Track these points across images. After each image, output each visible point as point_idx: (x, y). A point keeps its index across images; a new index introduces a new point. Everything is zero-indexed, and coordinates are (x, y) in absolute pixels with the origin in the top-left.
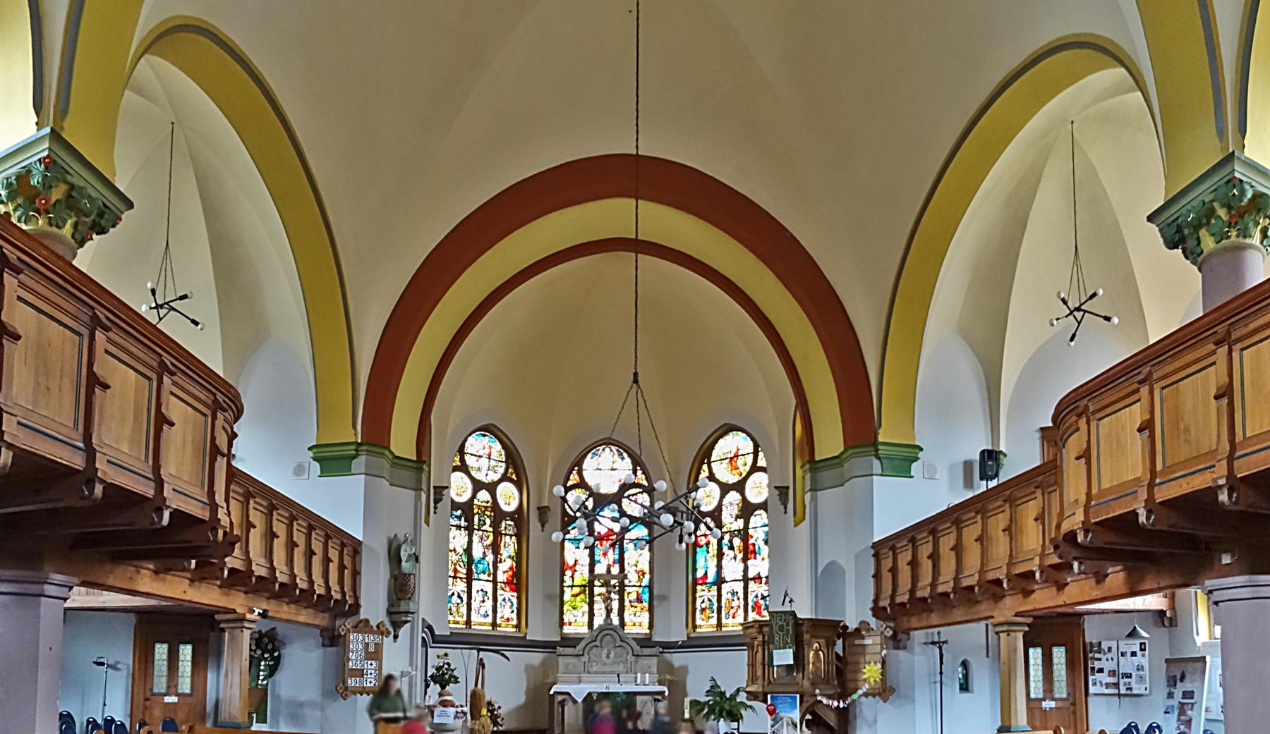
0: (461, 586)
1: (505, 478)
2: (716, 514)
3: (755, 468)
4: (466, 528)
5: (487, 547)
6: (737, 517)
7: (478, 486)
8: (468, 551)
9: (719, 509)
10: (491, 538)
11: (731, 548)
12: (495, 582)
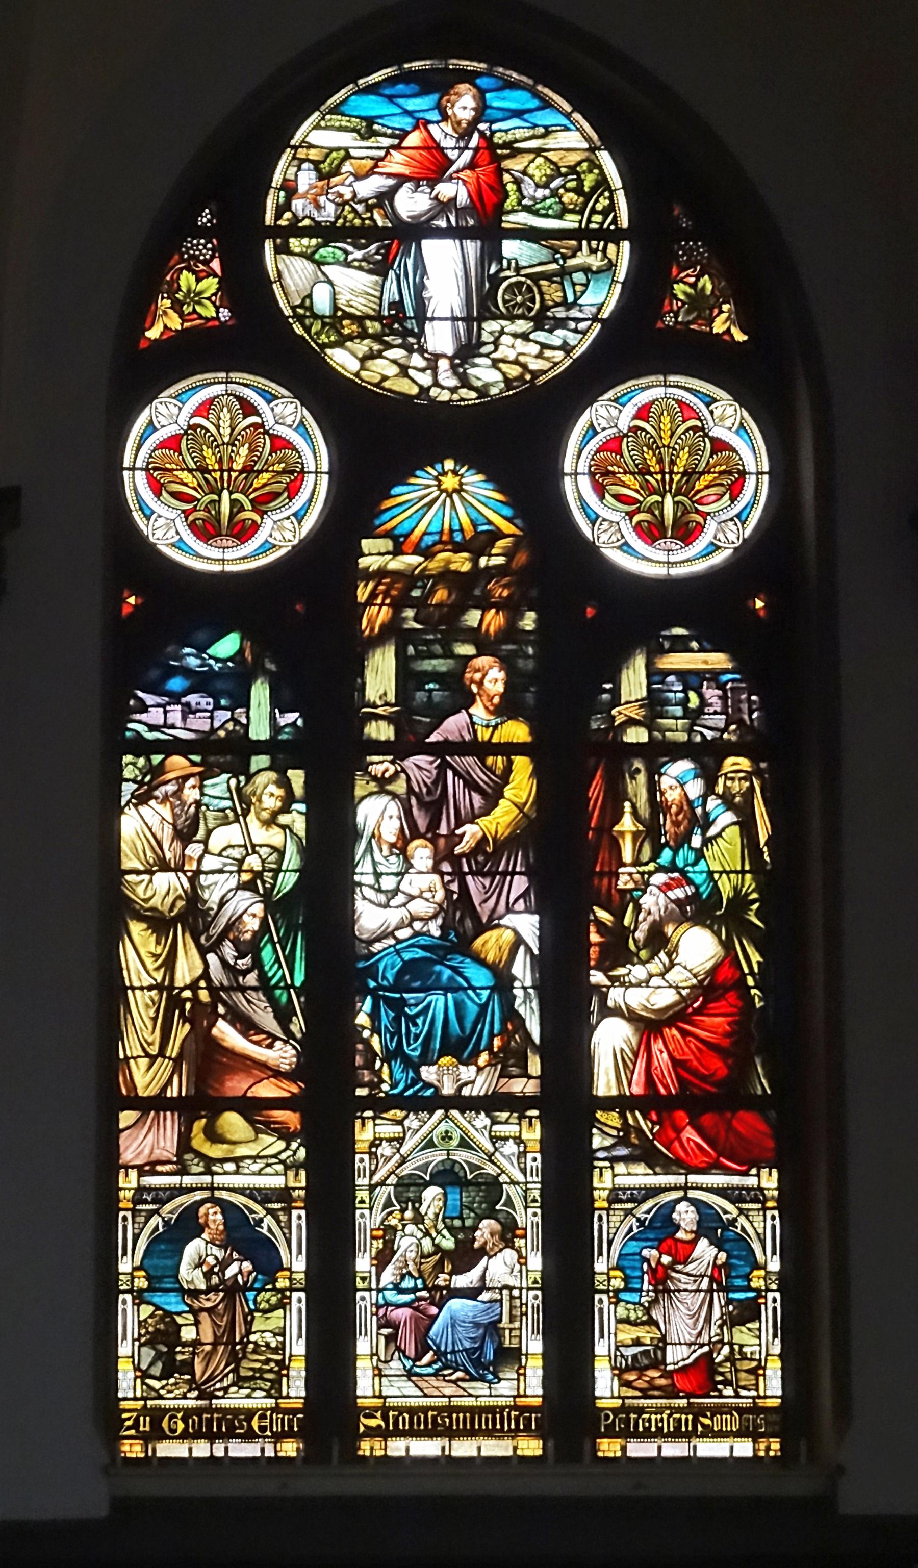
0: (257, 1162)
1: (633, 345)
4: (282, 751)
5: (488, 858)
7: (380, 441)
8: (318, 900)
10: (522, 784)
12: (566, 1106)
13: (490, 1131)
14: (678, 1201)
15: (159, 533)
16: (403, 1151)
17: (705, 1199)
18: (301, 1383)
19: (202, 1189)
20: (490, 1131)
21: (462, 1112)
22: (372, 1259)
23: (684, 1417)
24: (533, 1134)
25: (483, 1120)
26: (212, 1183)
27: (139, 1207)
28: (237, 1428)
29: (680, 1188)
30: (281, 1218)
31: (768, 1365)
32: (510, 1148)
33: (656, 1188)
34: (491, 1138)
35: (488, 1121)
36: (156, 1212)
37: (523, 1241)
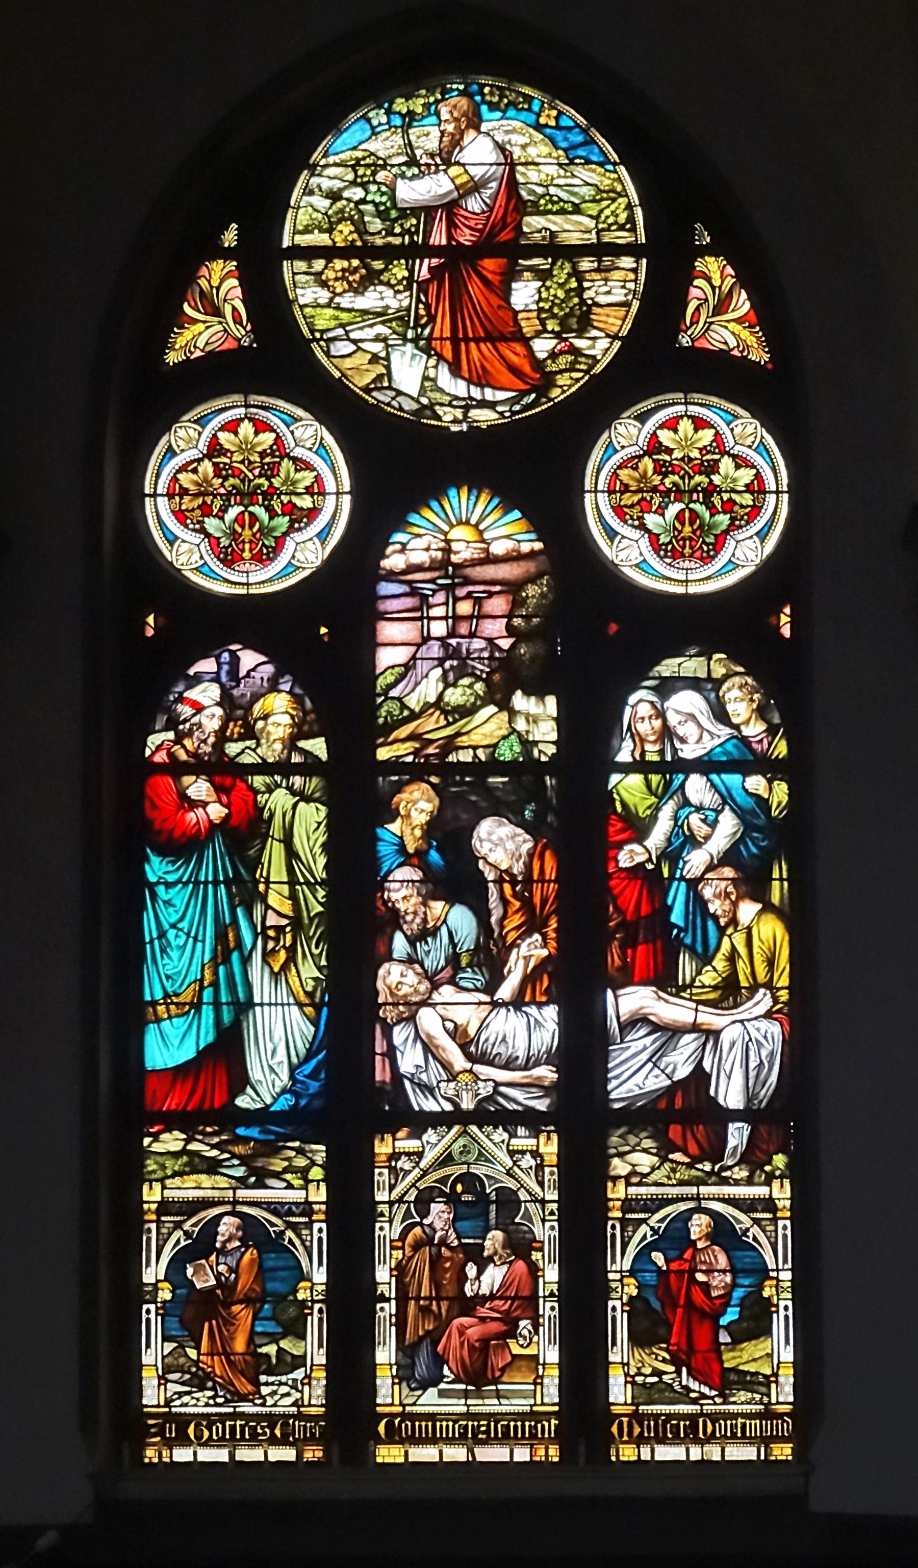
2: (322, 634)
3: (656, 361)
6: (505, 680)
9: (348, 589)
11: (456, 877)
13: (508, 1145)
14: (692, 1211)
15: (183, 559)
16: (423, 1164)
17: (721, 1211)
18: (789, 1389)
19: (687, 1199)
20: (508, 1145)
21: (480, 1128)
22: (391, 1270)
23: (512, 1424)
24: (550, 1148)
25: (500, 1135)
26: (698, 1194)
27: (628, 1216)
28: (260, 1435)
29: (228, 1203)
30: (768, 1228)
31: (780, 1372)
32: (528, 1161)
33: (208, 1202)
34: (509, 1151)
35: (506, 1136)
36: (644, 1221)
37: (539, 1255)
